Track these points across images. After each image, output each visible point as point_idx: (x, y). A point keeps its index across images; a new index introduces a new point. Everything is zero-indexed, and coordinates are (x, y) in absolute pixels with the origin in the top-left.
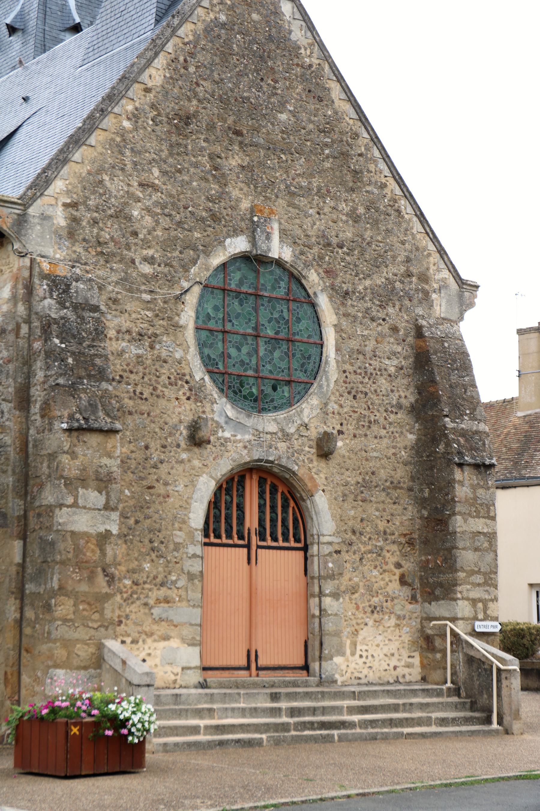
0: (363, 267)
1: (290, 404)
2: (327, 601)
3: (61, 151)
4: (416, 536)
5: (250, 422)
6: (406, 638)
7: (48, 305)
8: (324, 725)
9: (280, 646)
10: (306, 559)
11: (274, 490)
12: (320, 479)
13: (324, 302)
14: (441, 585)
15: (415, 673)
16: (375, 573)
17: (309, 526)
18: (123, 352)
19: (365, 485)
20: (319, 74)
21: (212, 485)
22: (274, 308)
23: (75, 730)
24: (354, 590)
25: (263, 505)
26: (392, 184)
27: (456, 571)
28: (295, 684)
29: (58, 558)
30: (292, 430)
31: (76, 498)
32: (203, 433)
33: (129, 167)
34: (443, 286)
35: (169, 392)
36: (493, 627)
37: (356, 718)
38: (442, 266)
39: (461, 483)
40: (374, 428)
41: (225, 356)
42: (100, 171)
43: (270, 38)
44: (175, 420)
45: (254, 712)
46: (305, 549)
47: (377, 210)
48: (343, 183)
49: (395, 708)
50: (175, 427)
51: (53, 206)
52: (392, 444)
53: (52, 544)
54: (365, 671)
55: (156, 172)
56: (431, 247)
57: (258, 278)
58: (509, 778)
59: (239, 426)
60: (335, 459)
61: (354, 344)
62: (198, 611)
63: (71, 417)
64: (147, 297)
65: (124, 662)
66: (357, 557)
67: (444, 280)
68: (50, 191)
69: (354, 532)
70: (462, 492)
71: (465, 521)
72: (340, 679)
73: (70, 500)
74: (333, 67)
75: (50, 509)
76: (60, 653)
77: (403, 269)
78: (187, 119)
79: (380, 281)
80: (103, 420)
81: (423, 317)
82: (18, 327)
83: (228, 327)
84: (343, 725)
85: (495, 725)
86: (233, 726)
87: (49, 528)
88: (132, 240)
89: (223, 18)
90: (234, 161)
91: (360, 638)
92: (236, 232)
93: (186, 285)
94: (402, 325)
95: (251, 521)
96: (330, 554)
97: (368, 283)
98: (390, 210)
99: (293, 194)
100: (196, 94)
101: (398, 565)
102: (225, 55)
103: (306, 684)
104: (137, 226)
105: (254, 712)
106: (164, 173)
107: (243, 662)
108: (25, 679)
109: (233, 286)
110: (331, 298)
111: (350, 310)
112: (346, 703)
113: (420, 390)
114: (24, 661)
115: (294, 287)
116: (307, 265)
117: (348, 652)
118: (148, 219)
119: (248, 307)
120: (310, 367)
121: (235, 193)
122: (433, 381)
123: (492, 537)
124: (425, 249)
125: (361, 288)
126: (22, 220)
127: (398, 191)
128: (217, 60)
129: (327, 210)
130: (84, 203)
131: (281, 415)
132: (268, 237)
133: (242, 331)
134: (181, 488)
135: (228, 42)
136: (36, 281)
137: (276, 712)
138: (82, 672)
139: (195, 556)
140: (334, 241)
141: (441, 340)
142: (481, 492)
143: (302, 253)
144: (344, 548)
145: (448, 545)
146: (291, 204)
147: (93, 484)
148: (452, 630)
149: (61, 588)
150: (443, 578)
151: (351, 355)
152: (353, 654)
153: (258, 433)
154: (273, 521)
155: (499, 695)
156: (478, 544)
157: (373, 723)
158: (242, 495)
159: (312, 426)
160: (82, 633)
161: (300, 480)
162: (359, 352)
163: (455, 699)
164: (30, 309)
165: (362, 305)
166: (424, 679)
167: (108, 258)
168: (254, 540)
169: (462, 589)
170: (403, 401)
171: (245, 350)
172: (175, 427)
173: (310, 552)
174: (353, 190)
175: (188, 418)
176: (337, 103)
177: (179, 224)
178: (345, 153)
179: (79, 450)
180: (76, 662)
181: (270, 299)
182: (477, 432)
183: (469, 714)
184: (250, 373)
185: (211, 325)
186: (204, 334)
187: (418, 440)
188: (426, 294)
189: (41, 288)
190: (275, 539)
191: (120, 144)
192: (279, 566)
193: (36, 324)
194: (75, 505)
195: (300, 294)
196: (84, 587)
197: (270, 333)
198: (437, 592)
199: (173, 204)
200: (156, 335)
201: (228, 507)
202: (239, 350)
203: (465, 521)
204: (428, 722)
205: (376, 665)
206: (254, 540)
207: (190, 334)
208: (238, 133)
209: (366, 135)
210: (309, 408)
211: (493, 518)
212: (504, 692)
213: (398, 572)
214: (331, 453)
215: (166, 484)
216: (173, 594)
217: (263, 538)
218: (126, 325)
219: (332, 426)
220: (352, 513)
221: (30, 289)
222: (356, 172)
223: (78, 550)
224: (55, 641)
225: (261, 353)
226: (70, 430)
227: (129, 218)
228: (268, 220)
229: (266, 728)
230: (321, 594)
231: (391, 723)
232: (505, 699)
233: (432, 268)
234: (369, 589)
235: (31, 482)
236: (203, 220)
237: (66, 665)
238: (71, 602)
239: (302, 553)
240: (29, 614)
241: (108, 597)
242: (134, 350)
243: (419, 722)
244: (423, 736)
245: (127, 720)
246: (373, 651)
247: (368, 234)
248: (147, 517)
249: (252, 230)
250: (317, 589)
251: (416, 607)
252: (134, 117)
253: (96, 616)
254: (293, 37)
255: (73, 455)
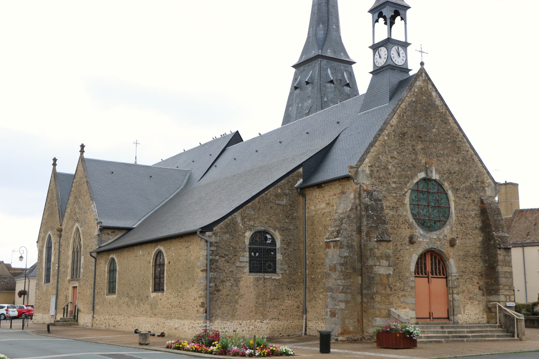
0: (462, 180)
1: (440, 228)
2: (455, 296)
3: (367, 149)
4: (483, 273)
5: (428, 235)
6: (481, 308)
7: (367, 200)
8: (460, 337)
9: (440, 311)
10: (447, 281)
11: (435, 258)
12: (451, 254)
13: (450, 193)
14: (494, 290)
15: (485, 320)
16: (470, 286)
17: (447, 270)
18: (388, 213)
19: (466, 256)
20: (445, 115)
21: (417, 257)
22: (433, 196)
23: (398, 335)
24: (463, 292)
25: (433, 263)
26: (471, 150)
27: (499, 285)
28: (446, 324)
29: (375, 282)
30: (441, 237)
31: (380, 263)
32: (414, 240)
33: (387, 152)
34: (489, 185)
35: (402, 226)
36: (513, 304)
37: (470, 335)
38: (489, 178)
39: (500, 255)
40: (468, 236)
41: (419, 213)
42: (379, 154)
43: (429, 105)
44: (405, 236)
45: (437, 332)
46: (446, 278)
47: (466, 159)
48: (454, 151)
49: (482, 332)
50: (405, 238)
51: (365, 168)
52: (473, 241)
53: (373, 278)
54: (468, 319)
55: (395, 153)
56: (485, 171)
57: (428, 186)
58: (533, 351)
59: (425, 237)
60: (456, 247)
61: (460, 207)
62: (414, 299)
63: (377, 237)
64: (394, 195)
65: (399, 316)
66: (464, 280)
67: (489, 183)
68: (364, 163)
69: (463, 272)
70: (500, 258)
71: (502, 268)
72: (460, 322)
73: (378, 264)
74: (450, 112)
75: (371, 267)
76: (378, 312)
77: (475, 179)
78: (404, 134)
79: (468, 184)
80: (386, 238)
81: (483, 196)
82: (357, 207)
83: (419, 203)
84: (466, 337)
85: (516, 338)
86: (432, 336)
87: (371, 273)
88: (389, 176)
89: (414, 99)
90: (419, 147)
91: (466, 308)
92: (421, 171)
93: (406, 190)
94: (476, 199)
95: (429, 269)
96: (455, 280)
97: (464, 185)
98: (470, 159)
99: (438, 156)
100: (407, 126)
101: (478, 283)
102: (415, 112)
103: (449, 324)
104: (390, 171)
105: (437, 332)
106: (398, 153)
107: (428, 316)
108: (365, 320)
109: (420, 189)
110: (452, 191)
111: (459, 195)
112: (466, 330)
113: (483, 222)
114: (364, 315)
115: (440, 188)
116: (444, 181)
117: (462, 313)
118: (394, 169)
119: (425, 196)
120: (446, 215)
121: (420, 158)
122: (488, 219)
123: (511, 273)
124: (483, 172)
125: (462, 187)
126: (357, 173)
127: (473, 153)
128: (413, 113)
129: (450, 161)
130: (374, 165)
131: (438, 232)
132: (432, 172)
133: (424, 204)
134: (407, 258)
135: (416, 107)
136: (362, 192)
137: (444, 332)
138: (384, 319)
139: (413, 281)
140: (452, 171)
141: (490, 204)
142: (507, 258)
143: (442, 176)
144: (460, 277)
145: (496, 276)
146: (438, 160)
147: (385, 258)
148: (499, 306)
149: (377, 292)
150: (494, 287)
151: (460, 210)
152: (464, 314)
153: (431, 239)
154: (436, 268)
155: (517, 328)
156: (506, 276)
157: (476, 336)
158: (425, 260)
159: (448, 236)
160: (383, 306)
161: (445, 254)
162: (462, 209)
163: (500, 329)
164: (360, 201)
165: (462, 193)
166: (488, 322)
167: (382, 182)
168: (430, 275)
169: (502, 291)
170: (477, 226)
171: (425, 211)
172: (405, 238)
173: (448, 279)
174: (458, 153)
175: (408, 235)
176: (451, 124)
177: (403, 169)
178: (454, 140)
179: (380, 247)
180: (382, 315)
181: (432, 193)
182: (504, 237)
183: (506, 334)
184: (427, 218)
185: (414, 203)
186: (412, 206)
187: (483, 239)
188: (484, 188)
189: (364, 195)
190: (436, 275)
191: (384, 144)
192: (438, 283)
193: (363, 206)
194: (380, 265)
195: (442, 190)
196: (383, 292)
197: (433, 204)
198: (492, 292)
199: (401, 163)
200: (397, 207)
201: (421, 264)
202: (423, 210)
203: (502, 268)
204: (493, 336)
205: (472, 317)
206: (430, 275)
207: (408, 207)
208: (420, 137)
209: (461, 134)
210: (446, 230)
211: (511, 267)
212: (519, 326)
213: (478, 285)
214: (455, 245)
215: (403, 257)
216: (406, 293)
217: (432, 274)
218: (389, 205)
219: (454, 236)
220: (462, 265)
221: (360, 195)
222: (459, 147)
223: (381, 280)
224: (376, 309)
225: (430, 211)
226: (377, 241)
227: (388, 169)
228: (431, 166)
229: (442, 337)
230: (453, 293)
231: (482, 336)
232: (519, 329)
233: (485, 179)
234: (468, 291)
235: (363, 258)
236: (410, 167)
237: (379, 316)
238: (380, 296)
239: (445, 280)
240: (365, 300)
241: (390, 295)
242: (391, 213)
243: (491, 336)
244: (493, 341)
245: (412, 332)
246: (471, 313)
247: (463, 168)
248: (397, 268)
249: (426, 170)
250: (451, 292)
251: (484, 298)
252: (388, 135)
253: (387, 301)
254: (436, 103)
255: (378, 249)
